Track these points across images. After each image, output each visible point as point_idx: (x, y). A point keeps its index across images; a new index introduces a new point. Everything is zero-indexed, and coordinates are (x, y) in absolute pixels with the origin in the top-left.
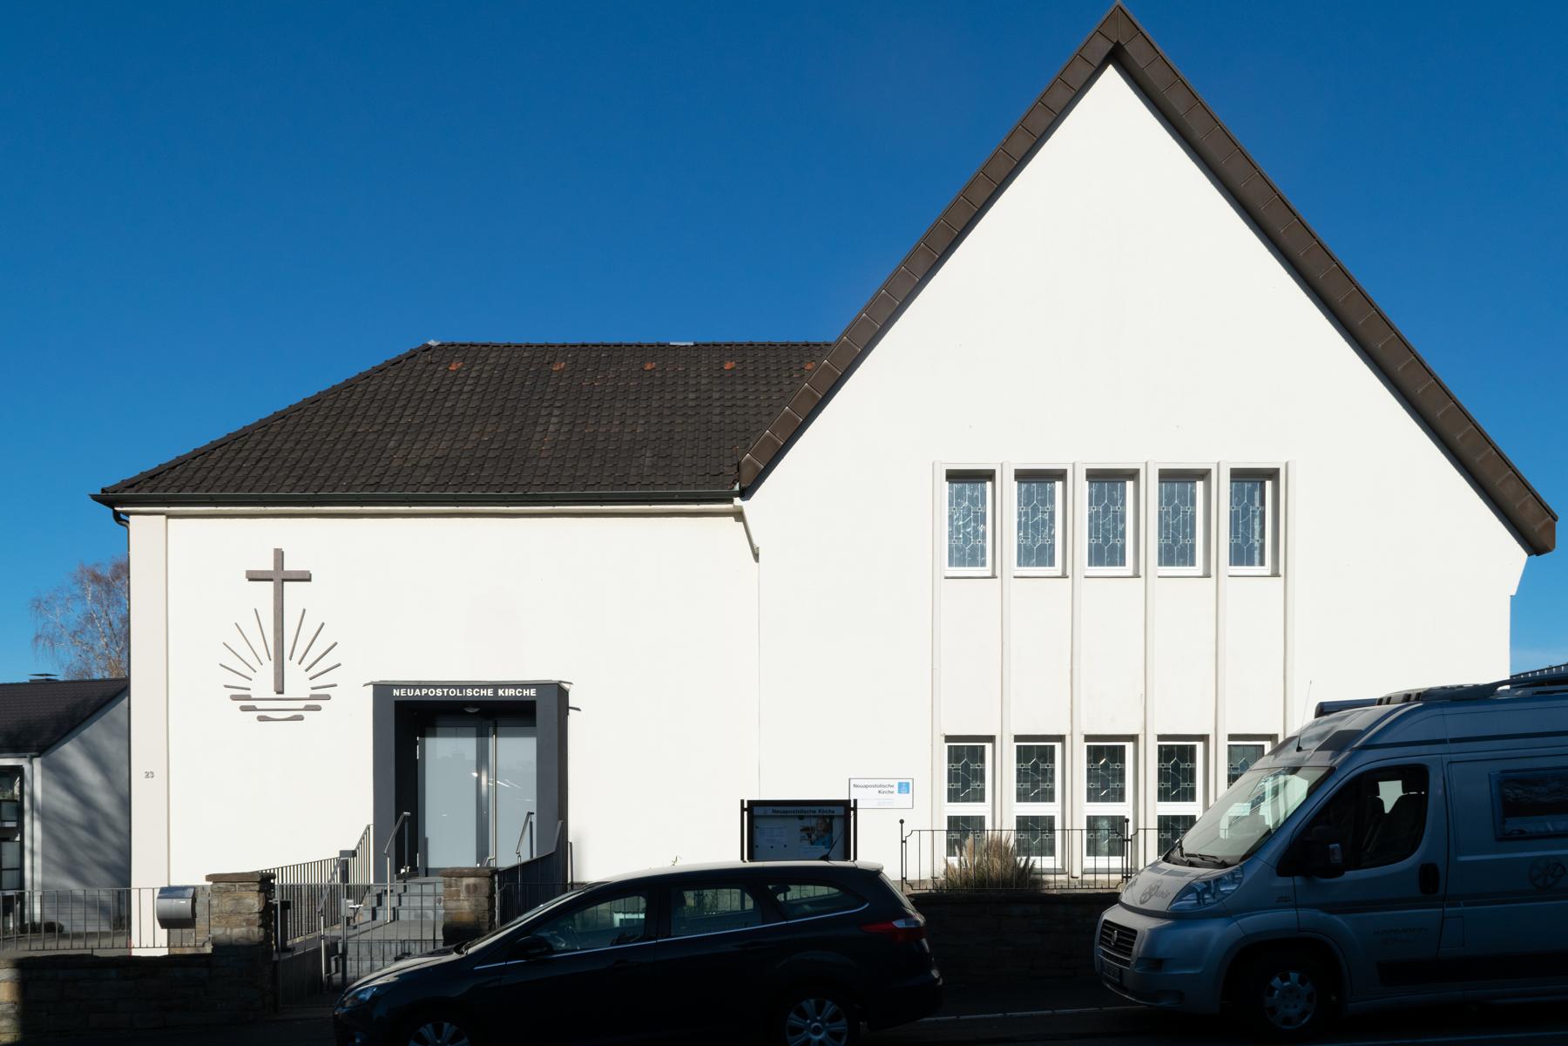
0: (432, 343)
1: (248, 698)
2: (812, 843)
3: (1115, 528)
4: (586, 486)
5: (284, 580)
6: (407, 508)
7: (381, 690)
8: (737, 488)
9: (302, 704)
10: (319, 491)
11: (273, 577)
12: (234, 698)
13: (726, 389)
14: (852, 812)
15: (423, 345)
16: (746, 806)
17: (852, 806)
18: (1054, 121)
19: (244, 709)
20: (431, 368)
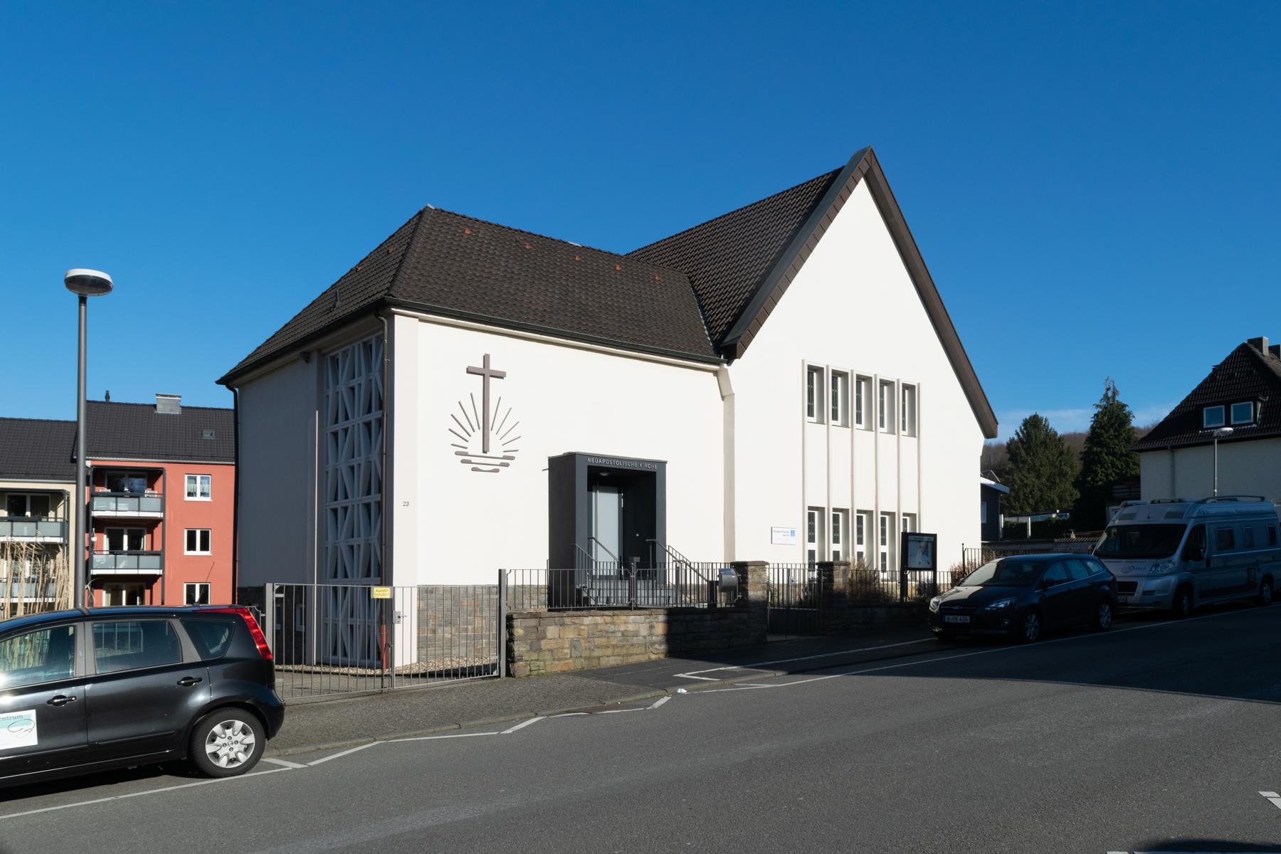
1: (466, 454)
7: (662, 464)
9: (498, 462)
12: (457, 453)
19: (463, 461)
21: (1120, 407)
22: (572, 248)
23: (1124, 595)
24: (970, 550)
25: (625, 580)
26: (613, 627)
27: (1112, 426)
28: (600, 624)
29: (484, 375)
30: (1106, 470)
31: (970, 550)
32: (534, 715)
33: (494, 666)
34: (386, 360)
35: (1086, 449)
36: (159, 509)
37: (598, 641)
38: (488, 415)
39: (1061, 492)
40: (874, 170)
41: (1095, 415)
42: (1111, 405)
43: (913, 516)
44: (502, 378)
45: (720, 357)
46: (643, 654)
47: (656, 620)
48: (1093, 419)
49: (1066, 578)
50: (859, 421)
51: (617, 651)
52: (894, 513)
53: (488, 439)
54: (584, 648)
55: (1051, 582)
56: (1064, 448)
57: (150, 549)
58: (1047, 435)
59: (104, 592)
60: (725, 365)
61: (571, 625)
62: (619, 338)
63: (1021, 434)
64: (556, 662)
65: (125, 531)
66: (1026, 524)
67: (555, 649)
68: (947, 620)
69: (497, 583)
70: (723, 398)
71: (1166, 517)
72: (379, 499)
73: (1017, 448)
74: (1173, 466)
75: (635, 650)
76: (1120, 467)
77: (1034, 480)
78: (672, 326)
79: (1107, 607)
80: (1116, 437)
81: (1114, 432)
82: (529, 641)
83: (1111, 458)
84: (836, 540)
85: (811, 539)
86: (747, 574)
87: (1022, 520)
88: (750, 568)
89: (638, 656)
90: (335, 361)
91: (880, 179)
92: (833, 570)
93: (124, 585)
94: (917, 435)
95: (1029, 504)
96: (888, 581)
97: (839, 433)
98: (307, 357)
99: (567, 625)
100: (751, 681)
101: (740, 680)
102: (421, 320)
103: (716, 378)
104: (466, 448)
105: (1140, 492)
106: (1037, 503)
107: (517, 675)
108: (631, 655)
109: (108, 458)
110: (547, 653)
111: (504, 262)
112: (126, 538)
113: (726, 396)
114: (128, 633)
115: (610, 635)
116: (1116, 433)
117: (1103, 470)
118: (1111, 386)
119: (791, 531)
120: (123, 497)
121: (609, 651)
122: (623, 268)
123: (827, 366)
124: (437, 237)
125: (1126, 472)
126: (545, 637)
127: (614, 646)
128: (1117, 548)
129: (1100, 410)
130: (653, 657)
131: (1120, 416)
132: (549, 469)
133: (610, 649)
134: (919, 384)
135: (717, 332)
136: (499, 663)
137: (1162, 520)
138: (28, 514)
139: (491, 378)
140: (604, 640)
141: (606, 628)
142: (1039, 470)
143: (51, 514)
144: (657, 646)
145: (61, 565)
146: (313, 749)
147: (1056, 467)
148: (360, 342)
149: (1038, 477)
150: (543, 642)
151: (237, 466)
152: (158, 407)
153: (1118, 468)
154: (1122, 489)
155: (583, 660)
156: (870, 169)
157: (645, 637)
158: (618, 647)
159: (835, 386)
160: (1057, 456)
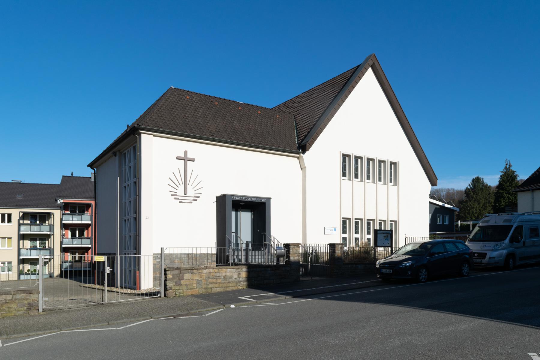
1: (176, 195)
2: (385, 239)
6: (236, 146)
7: (269, 199)
12: (172, 195)
19: (175, 199)
21: (512, 172)
22: (238, 104)
23: (481, 259)
24: (409, 238)
25: (259, 251)
26: (219, 274)
27: (508, 181)
28: (212, 273)
29: (184, 160)
30: (505, 200)
31: (409, 238)
32: (150, 318)
33: (158, 293)
34: (138, 154)
35: (496, 191)
36: (89, 220)
37: (211, 280)
38: (187, 178)
39: (489, 210)
40: (376, 64)
41: (501, 176)
42: (508, 171)
43: (395, 222)
44: (194, 161)
45: (300, 151)
46: (235, 286)
47: (242, 271)
48: (500, 178)
49: (444, 251)
50: (391, 182)
51: (221, 285)
52: (396, 221)
53: (187, 189)
54: (203, 284)
55: (435, 254)
56: (491, 191)
57: (87, 237)
58: (483, 186)
59: (69, 254)
60: (302, 154)
61: (197, 273)
62: (250, 142)
63: (471, 185)
64: (189, 290)
65: (77, 229)
66: (469, 225)
67: (189, 284)
68: (382, 272)
69: (160, 253)
70: (302, 169)
71: (503, 222)
72: (135, 216)
73: (469, 191)
74: (533, 198)
75: (230, 285)
76: (512, 199)
77: (477, 205)
78: (293, 138)
79: (467, 266)
80: (510, 186)
81: (510, 184)
82: (175, 281)
83: (508, 195)
84: (357, 232)
85: (344, 232)
86: (290, 249)
87: (468, 223)
88: (291, 247)
89: (232, 287)
90: (125, 154)
91: (378, 68)
92: (335, 247)
93: (77, 251)
94: (397, 185)
95: (474, 216)
96: (382, 251)
97: (357, 183)
98: (115, 154)
99: (195, 273)
100: (268, 302)
101: (263, 301)
102: (154, 136)
103: (298, 160)
104: (176, 193)
105: (517, 210)
106: (478, 216)
107: (168, 296)
108: (228, 287)
109: (70, 199)
110: (184, 286)
111: (269, 120)
112: (77, 232)
113: (303, 168)
114: (68, 271)
115: (218, 278)
116: (510, 184)
117: (504, 200)
118: (508, 163)
119: (334, 229)
120: (75, 215)
121: (217, 285)
122: (262, 113)
123: (352, 154)
124: (196, 105)
125: (515, 201)
126: (183, 279)
127: (219, 283)
128: (482, 236)
129: (503, 174)
130: (240, 288)
131: (513, 176)
132: (217, 202)
133: (217, 284)
134: (398, 162)
135: (300, 140)
136: (161, 291)
137: (502, 223)
138: (38, 222)
139: (188, 161)
140: (214, 280)
141: (215, 274)
142: (479, 201)
143: (47, 222)
144: (242, 283)
146: (26, 335)
147: (487, 199)
148: (132, 147)
149: (479, 204)
150: (182, 282)
151: (95, 201)
152: (92, 178)
153: (511, 200)
154: (510, 209)
155: (203, 289)
156: (374, 63)
157: (236, 279)
158: (221, 283)
159: (380, 167)
160: (488, 194)
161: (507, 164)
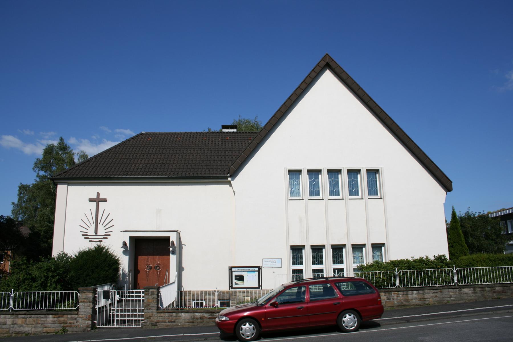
0: (143, 132)
1: (87, 235)
3: (75, 334)
4: (186, 174)
5: (99, 201)
8: (229, 175)
9: (102, 237)
10: (111, 176)
11: (96, 200)
12: (83, 235)
13: (226, 145)
14: (260, 270)
15: (141, 133)
16: (230, 268)
17: (260, 268)
18: (302, 92)
19: (85, 238)
20: (142, 139)
104: (87, 232)
145: (98, 243)
161: (234, 121)
